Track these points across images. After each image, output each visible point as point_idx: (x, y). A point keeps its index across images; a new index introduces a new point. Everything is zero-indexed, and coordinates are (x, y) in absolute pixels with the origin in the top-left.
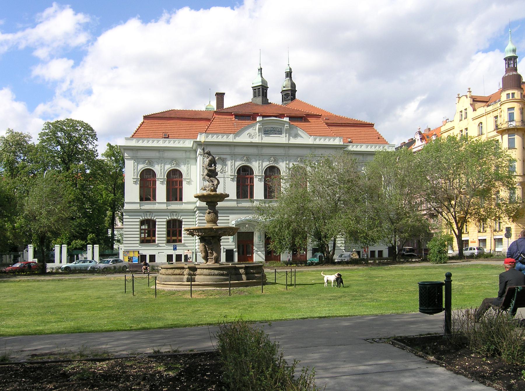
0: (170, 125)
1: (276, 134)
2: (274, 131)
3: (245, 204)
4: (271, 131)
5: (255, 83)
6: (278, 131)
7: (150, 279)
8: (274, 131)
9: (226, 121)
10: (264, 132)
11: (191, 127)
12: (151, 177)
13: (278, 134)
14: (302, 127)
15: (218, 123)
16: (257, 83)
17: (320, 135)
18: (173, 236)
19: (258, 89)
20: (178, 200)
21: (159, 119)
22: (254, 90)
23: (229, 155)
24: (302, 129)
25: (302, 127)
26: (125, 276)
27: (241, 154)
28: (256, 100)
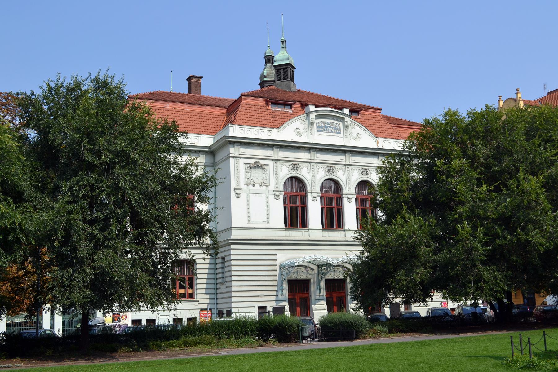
0: (169, 112)
1: (332, 132)
2: (330, 127)
3: (334, 235)
4: (326, 127)
5: (279, 61)
6: (335, 129)
7: (508, 343)
8: (330, 127)
9: (259, 110)
10: (317, 128)
11: (199, 117)
12: (332, 191)
13: (335, 133)
14: (363, 123)
15: (249, 111)
16: (281, 60)
17: (208, 131)
18: (180, 288)
19: (284, 69)
20: (299, 227)
21: (211, 107)
22: (277, 70)
23: (273, 160)
24: (367, 128)
25: (363, 123)
26: (544, 332)
27: (224, 159)
28: (281, 85)
